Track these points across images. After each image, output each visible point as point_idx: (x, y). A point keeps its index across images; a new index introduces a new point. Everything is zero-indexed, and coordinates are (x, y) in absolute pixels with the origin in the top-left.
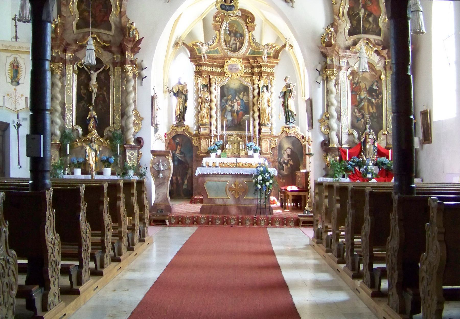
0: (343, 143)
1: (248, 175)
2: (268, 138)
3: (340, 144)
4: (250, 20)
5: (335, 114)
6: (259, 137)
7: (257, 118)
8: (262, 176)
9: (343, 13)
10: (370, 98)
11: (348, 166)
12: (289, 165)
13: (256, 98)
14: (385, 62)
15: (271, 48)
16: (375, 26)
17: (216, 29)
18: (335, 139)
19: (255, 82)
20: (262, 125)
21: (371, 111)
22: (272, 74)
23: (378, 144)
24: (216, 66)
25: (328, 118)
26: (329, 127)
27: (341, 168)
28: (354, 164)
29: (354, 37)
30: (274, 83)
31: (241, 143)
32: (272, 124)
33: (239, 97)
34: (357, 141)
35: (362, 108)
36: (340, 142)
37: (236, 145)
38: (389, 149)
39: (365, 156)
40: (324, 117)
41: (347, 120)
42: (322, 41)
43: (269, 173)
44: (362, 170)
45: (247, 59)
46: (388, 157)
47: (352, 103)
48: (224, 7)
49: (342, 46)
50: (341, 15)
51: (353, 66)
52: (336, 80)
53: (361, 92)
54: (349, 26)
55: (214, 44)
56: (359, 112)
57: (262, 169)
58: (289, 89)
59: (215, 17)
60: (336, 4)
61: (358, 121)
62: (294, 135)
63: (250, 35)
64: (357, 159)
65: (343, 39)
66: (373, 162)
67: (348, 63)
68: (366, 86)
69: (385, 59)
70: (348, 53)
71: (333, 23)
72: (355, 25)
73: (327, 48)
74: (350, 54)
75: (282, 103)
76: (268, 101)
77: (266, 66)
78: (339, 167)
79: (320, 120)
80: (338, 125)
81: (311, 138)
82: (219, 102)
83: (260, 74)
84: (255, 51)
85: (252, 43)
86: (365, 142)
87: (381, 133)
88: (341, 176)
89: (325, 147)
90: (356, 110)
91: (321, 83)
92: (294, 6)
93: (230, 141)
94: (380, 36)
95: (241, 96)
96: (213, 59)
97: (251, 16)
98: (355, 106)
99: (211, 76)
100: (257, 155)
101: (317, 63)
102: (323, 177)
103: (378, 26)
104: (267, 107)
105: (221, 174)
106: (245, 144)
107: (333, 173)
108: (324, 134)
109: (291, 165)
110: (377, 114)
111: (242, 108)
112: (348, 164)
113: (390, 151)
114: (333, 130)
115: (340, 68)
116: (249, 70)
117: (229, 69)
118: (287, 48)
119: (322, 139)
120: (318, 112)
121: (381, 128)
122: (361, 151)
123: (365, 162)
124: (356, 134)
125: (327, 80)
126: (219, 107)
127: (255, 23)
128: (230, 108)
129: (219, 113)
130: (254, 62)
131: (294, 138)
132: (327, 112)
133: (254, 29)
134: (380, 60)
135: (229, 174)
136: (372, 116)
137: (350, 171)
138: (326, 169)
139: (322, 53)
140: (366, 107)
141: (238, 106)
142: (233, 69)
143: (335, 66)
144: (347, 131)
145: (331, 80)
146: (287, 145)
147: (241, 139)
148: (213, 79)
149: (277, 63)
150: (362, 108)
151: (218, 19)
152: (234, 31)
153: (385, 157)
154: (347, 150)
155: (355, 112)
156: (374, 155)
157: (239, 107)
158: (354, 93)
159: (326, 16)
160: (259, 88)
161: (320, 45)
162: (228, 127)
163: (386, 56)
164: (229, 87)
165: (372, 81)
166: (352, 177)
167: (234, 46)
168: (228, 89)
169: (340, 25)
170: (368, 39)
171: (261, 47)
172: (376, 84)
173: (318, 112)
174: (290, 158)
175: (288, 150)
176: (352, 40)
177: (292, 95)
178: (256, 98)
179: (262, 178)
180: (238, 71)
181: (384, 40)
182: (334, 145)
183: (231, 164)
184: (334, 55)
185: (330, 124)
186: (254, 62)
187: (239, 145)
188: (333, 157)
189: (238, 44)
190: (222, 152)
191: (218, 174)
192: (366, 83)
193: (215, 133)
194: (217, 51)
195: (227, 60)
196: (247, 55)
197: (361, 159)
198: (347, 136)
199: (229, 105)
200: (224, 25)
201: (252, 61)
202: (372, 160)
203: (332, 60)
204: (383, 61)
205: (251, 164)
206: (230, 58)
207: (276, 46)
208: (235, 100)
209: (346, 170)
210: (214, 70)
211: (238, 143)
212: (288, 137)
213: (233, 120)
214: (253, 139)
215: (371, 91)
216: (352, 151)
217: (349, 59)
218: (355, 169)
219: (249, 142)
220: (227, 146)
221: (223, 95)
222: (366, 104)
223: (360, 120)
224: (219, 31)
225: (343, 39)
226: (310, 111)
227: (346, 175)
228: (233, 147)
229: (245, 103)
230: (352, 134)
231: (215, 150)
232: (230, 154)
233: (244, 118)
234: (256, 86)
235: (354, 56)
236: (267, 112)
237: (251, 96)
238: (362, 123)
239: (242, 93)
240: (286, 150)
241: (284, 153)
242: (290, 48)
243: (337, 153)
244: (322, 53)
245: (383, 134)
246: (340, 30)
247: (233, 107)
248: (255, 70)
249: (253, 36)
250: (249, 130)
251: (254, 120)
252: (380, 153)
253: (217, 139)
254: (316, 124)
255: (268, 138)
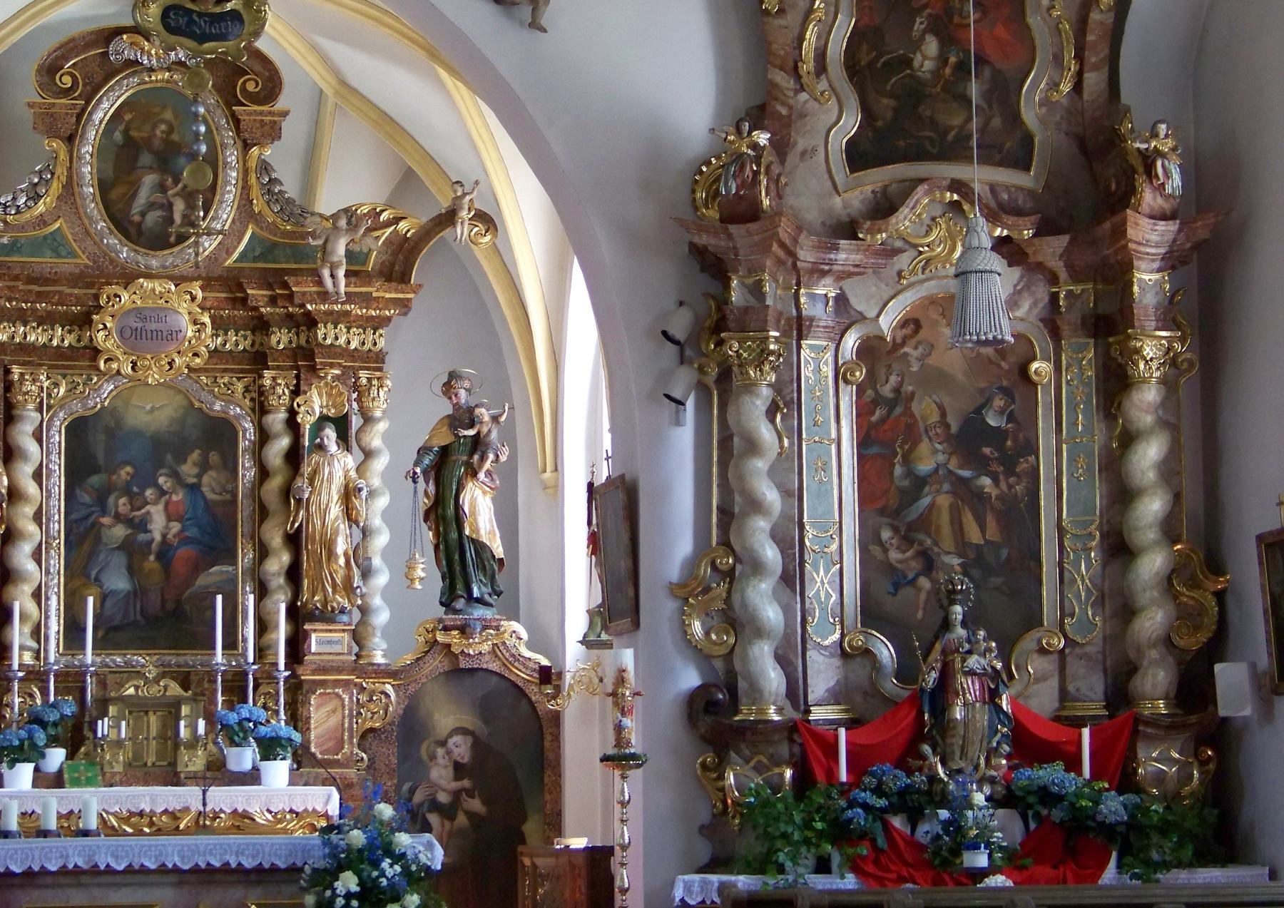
0: (811, 698)
1: (274, 869)
2: (346, 685)
3: (795, 706)
4: (251, 87)
5: (771, 554)
6: (294, 675)
7: (278, 582)
8: (358, 873)
9: (821, 56)
10: (966, 473)
11: (849, 813)
12: (462, 819)
13: (275, 483)
14: (1054, 298)
15: (369, 230)
16: (996, 122)
17: (52, 133)
18: (773, 678)
19: (273, 401)
20: (312, 618)
21: (974, 534)
22: (376, 360)
23: (1013, 701)
24: (47, 320)
25: (730, 575)
26: (737, 622)
27: (807, 824)
28: (882, 802)
29: (877, 178)
30: (380, 404)
31: (185, 710)
32: (364, 610)
33: (175, 475)
34: (891, 685)
35: (925, 522)
36: (796, 692)
37: (154, 720)
38: (1078, 723)
39: (944, 764)
40: (705, 570)
41: (835, 580)
42: (701, 195)
43: (399, 858)
44: (925, 831)
45: (228, 286)
46: (1073, 764)
47: (865, 498)
48: (183, 21)
49: (812, 215)
50: (808, 66)
51: (871, 314)
52: (777, 388)
53: (915, 443)
54: (850, 123)
55: (41, 208)
56: (907, 540)
57: (357, 837)
58: (471, 432)
59: (50, 69)
60: (781, 11)
61: (897, 586)
62: (494, 666)
63: (252, 164)
64: (897, 779)
65: (818, 179)
66: (987, 789)
67: (842, 300)
68: (943, 415)
69: (1053, 279)
70: (846, 254)
71: (762, 108)
72: (889, 115)
73: (733, 228)
74: (856, 258)
75: (424, 503)
76: (349, 494)
77: (337, 318)
78: (798, 818)
79: (682, 585)
80: (787, 610)
81: (631, 674)
82: (58, 506)
83: (305, 361)
84: (275, 244)
85: (258, 205)
86: (943, 692)
87: (1028, 642)
88: (811, 862)
89: (708, 719)
90: (886, 534)
91: (690, 404)
92: (543, 22)
93: (122, 700)
94: (1028, 169)
95: (188, 470)
96: (31, 280)
97: (258, 67)
98: (882, 512)
99: (16, 370)
100: (278, 771)
101: (670, 302)
102: (700, 871)
103: (1014, 118)
104: (343, 527)
105: (109, 871)
106: (211, 718)
107: (760, 848)
108: (700, 655)
109: (470, 815)
110: (1004, 553)
111: (192, 532)
112: (852, 804)
113: (1086, 732)
114: (759, 632)
115: (799, 327)
116: (236, 341)
117: (121, 333)
118: (463, 229)
119: (690, 679)
120: (674, 539)
121: (1033, 620)
122: (918, 736)
123: (944, 793)
124: (885, 652)
125: (723, 386)
126: (58, 525)
127: (281, 104)
128: (120, 532)
129: (57, 562)
130: (273, 301)
131: (495, 679)
132: (725, 543)
133: (273, 132)
134: (1027, 287)
135: (162, 870)
136: (975, 561)
137: (863, 835)
138: (713, 829)
139: (698, 252)
140: (945, 518)
141: (169, 518)
142: (145, 333)
143: (771, 318)
144: (837, 636)
145: (750, 387)
146: (448, 716)
147: (186, 687)
148: (28, 386)
149: (405, 306)
150: (925, 522)
151: (68, 81)
152: (157, 143)
153: (1059, 766)
154: (842, 732)
155: (880, 542)
156: (992, 753)
157: (176, 527)
158: (874, 450)
159: (724, 72)
160: (292, 424)
161: (688, 215)
162: (108, 631)
163: (1058, 266)
164: (119, 424)
165: (982, 391)
166: (870, 869)
167: (153, 217)
168: (111, 433)
169: (802, 116)
170: (956, 185)
171: (311, 224)
172: (998, 402)
173: (674, 539)
174: (466, 783)
175: (457, 739)
176: (869, 188)
177: (487, 465)
178: (275, 483)
179: (361, 883)
180: (173, 347)
181: (1047, 186)
182: (762, 711)
183: (126, 820)
184: (768, 263)
185: (744, 605)
186: (273, 301)
187: (177, 718)
188: (759, 769)
189: (179, 207)
190: (70, 756)
191: (94, 871)
192: (946, 400)
193: (28, 658)
194: (55, 244)
195: (114, 289)
196: (229, 262)
197: (919, 779)
198: (837, 662)
199: (118, 517)
200: (103, 111)
201: (256, 294)
202: (981, 782)
203: (757, 290)
204: (1042, 292)
205: (246, 815)
206: (128, 278)
207: (397, 220)
208: (149, 493)
209: (841, 832)
210: (31, 338)
211: (171, 710)
212: (459, 673)
213: (138, 592)
214: (256, 688)
215: (970, 439)
216: (863, 737)
217: (847, 285)
218: (887, 827)
219: (230, 705)
220: (103, 727)
221: (80, 465)
222: (944, 501)
223: (913, 582)
224: (70, 140)
225: (818, 179)
226: (625, 537)
227: (836, 859)
228: (135, 731)
229: (209, 505)
230: (867, 653)
231: (34, 746)
232: (119, 768)
233: (202, 580)
234: (277, 419)
235: (877, 270)
236: (341, 547)
237: (247, 471)
238: (923, 597)
239: (195, 455)
240: (443, 743)
241: (433, 757)
242: (481, 227)
243: (784, 750)
244: (698, 252)
245: (1042, 651)
246: (801, 143)
247: (141, 525)
248: (274, 339)
249: (265, 167)
250: (231, 643)
251: (262, 591)
252: (1028, 744)
253: (45, 693)
254: (657, 607)
255: (346, 685)
